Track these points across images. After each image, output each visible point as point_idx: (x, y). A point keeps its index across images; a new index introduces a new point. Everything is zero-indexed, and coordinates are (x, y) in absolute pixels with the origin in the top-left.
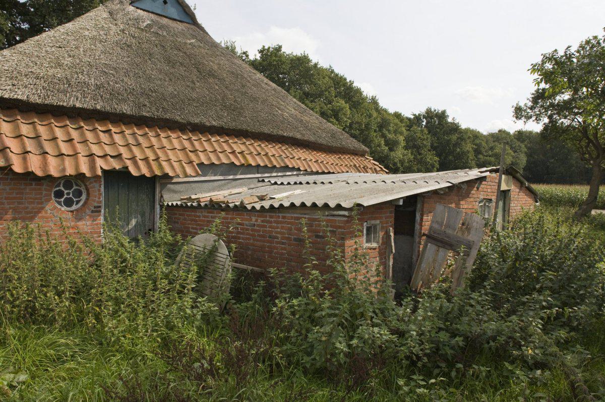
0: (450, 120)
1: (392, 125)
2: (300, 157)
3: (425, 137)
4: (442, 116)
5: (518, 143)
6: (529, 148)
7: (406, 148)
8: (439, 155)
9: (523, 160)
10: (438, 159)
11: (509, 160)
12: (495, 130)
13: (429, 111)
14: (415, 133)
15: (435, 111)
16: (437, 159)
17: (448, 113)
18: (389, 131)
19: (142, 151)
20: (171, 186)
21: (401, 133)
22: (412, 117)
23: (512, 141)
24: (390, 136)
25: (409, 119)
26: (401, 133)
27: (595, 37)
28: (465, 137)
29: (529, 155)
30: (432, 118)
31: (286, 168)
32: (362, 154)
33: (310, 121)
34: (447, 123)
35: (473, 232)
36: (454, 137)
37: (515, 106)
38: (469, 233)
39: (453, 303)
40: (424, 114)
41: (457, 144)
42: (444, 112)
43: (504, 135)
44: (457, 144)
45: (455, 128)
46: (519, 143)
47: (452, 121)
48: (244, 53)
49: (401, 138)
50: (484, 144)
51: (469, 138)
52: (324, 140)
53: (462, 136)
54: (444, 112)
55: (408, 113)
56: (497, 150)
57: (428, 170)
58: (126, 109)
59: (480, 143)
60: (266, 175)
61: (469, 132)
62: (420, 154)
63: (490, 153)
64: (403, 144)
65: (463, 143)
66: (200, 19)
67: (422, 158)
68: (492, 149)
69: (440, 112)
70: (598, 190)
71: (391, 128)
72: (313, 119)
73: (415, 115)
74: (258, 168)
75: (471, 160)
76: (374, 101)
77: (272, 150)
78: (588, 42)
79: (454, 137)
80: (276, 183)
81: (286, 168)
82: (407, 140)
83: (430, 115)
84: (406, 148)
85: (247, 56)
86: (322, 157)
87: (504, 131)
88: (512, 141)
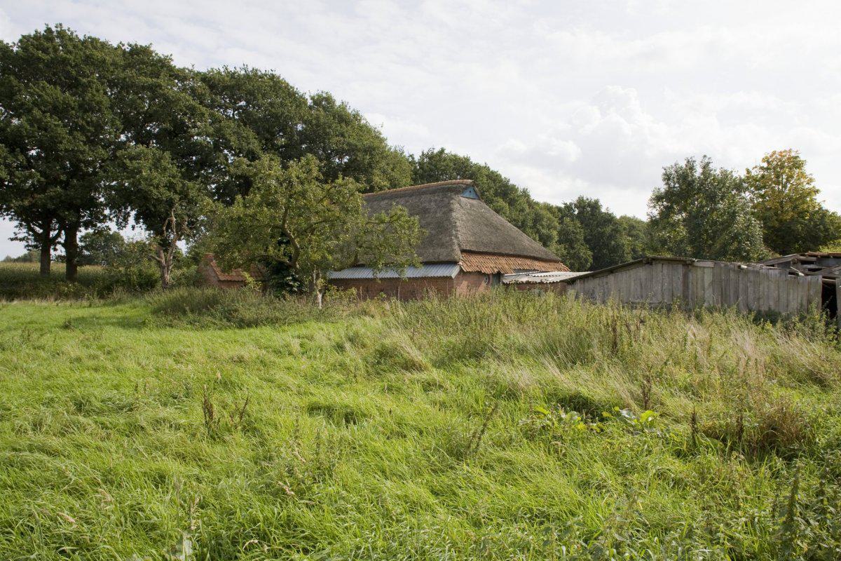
0: (603, 210)
1: (545, 220)
2: (537, 264)
3: (578, 230)
4: (595, 206)
7: (560, 242)
8: (592, 249)
10: (592, 253)
13: (581, 201)
14: (568, 227)
15: (588, 199)
16: (590, 253)
17: (601, 203)
18: (542, 225)
19: (489, 265)
21: (555, 228)
22: (563, 206)
24: (544, 231)
25: (559, 209)
26: (555, 228)
28: (620, 228)
30: (584, 208)
31: (535, 270)
34: (600, 213)
36: (608, 229)
40: (576, 202)
41: (611, 237)
42: (597, 202)
44: (611, 237)
45: (609, 219)
48: (411, 156)
49: (555, 233)
51: (625, 229)
54: (597, 202)
55: (558, 202)
57: (836, 298)
58: (491, 250)
62: (573, 248)
64: (556, 238)
65: (618, 235)
67: (575, 253)
69: (593, 200)
70: (49, 233)
71: (544, 223)
73: (566, 204)
74: (526, 270)
75: (627, 254)
76: (525, 194)
77: (528, 262)
79: (608, 229)
81: (535, 270)
82: (560, 233)
83: (581, 204)
84: (560, 242)
85: (413, 158)
86: (543, 264)
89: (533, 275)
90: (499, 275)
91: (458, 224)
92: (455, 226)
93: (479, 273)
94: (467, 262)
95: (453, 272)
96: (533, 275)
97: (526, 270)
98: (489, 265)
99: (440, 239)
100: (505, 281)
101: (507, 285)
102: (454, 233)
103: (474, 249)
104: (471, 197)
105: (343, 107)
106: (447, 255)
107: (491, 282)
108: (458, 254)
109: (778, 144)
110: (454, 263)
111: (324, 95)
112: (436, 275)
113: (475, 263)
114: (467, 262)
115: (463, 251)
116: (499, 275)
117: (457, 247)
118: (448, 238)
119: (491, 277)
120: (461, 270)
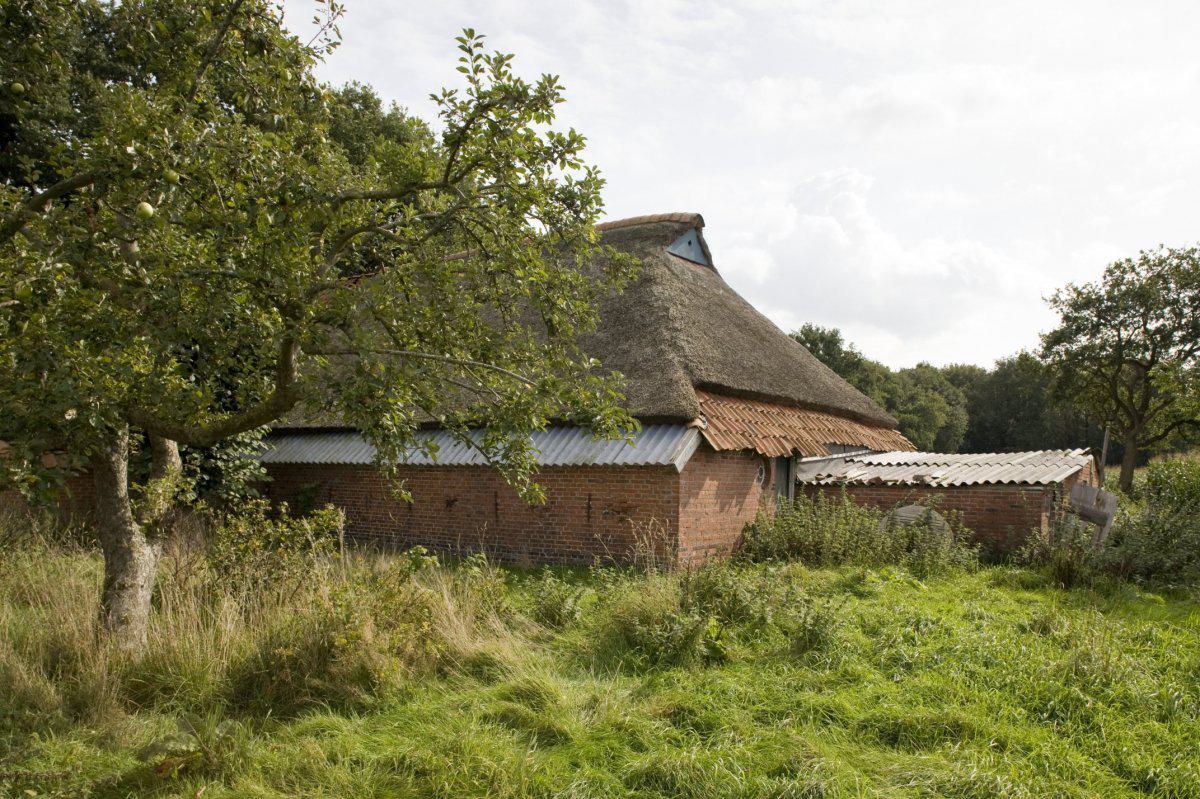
0: (845, 347)
2: (864, 434)
5: (952, 389)
6: (970, 398)
9: (963, 419)
11: (942, 420)
12: (911, 365)
15: (818, 329)
17: (842, 335)
19: (772, 432)
20: (802, 467)
23: (941, 383)
27: (1129, 260)
28: (873, 377)
29: (971, 411)
32: (887, 426)
33: (844, 390)
35: (1107, 506)
37: (1020, 352)
38: (1104, 507)
39: (180, 779)
42: (834, 335)
43: (928, 374)
46: (954, 388)
47: (849, 350)
50: (900, 391)
52: (862, 410)
53: (868, 376)
54: (834, 335)
56: (922, 402)
59: (894, 389)
60: (853, 454)
61: (877, 370)
63: (910, 407)
66: (716, 262)
68: (912, 399)
72: (848, 388)
78: (1118, 266)
80: (870, 464)
81: (863, 447)
87: (928, 366)
88: (941, 383)
89: (867, 459)
90: (788, 463)
91: (672, 311)
92: (667, 318)
93: (750, 455)
94: (714, 420)
95: (680, 450)
96: (867, 459)
97: (845, 448)
98: (772, 432)
99: (626, 352)
100: (804, 478)
101: (811, 489)
102: (666, 334)
103: (728, 382)
104: (693, 259)
105: (396, 116)
106: (653, 399)
107: (773, 480)
108: (690, 398)
109: (837, 327)
110: (679, 422)
111: (359, 90)
112: (619, 461)
113: (730, 426)
114: (714, 420)
115: (702, 387)
116: (788, 463)
117: (681, 373)
118: (648, 350)
119: (773, 465)
120: (704, 447)
